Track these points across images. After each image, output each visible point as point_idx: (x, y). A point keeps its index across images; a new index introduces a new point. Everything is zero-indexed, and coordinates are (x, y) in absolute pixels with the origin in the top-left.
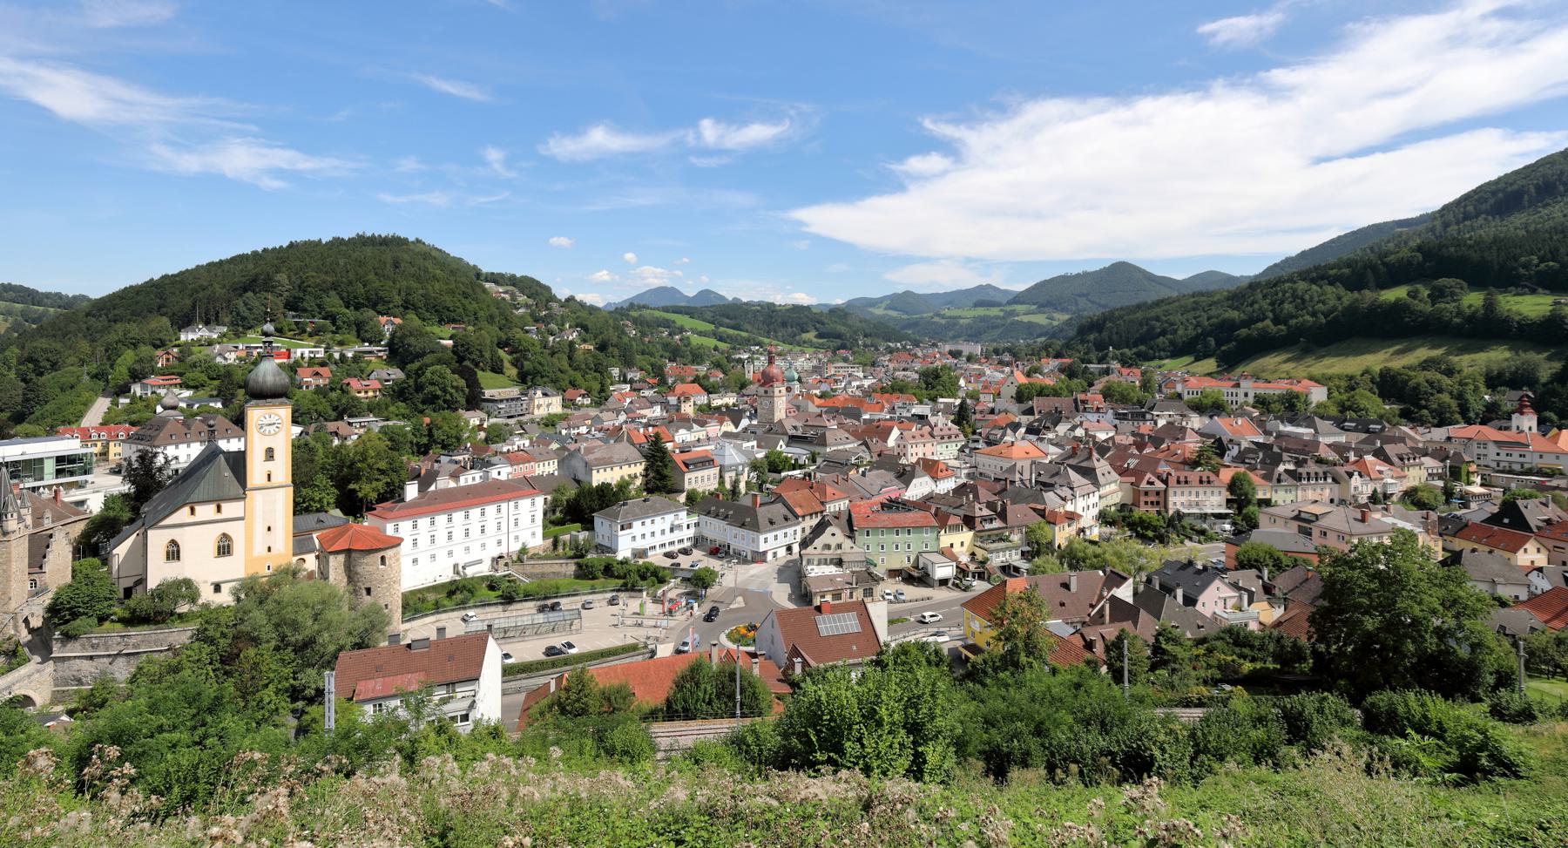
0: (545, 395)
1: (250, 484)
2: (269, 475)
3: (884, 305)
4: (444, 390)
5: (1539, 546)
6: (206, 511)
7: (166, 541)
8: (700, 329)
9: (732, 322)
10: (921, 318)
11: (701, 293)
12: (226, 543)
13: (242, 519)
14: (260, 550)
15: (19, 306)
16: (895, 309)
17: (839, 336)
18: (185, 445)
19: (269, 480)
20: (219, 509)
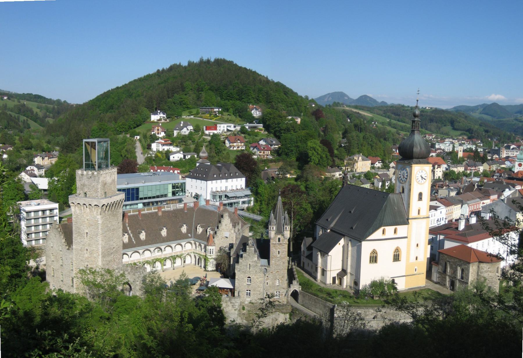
2: (419, 210)
3: (478, 111)
5: (350, 239)
6: (390, 230)
7: (370, 251)
12: (398, 253)
13: (406, 237)
14: (412, 259)
15: (44, 105)
16: (487, 114)
18: (225, 180)
19: (419, 214)
20: (395, 232)
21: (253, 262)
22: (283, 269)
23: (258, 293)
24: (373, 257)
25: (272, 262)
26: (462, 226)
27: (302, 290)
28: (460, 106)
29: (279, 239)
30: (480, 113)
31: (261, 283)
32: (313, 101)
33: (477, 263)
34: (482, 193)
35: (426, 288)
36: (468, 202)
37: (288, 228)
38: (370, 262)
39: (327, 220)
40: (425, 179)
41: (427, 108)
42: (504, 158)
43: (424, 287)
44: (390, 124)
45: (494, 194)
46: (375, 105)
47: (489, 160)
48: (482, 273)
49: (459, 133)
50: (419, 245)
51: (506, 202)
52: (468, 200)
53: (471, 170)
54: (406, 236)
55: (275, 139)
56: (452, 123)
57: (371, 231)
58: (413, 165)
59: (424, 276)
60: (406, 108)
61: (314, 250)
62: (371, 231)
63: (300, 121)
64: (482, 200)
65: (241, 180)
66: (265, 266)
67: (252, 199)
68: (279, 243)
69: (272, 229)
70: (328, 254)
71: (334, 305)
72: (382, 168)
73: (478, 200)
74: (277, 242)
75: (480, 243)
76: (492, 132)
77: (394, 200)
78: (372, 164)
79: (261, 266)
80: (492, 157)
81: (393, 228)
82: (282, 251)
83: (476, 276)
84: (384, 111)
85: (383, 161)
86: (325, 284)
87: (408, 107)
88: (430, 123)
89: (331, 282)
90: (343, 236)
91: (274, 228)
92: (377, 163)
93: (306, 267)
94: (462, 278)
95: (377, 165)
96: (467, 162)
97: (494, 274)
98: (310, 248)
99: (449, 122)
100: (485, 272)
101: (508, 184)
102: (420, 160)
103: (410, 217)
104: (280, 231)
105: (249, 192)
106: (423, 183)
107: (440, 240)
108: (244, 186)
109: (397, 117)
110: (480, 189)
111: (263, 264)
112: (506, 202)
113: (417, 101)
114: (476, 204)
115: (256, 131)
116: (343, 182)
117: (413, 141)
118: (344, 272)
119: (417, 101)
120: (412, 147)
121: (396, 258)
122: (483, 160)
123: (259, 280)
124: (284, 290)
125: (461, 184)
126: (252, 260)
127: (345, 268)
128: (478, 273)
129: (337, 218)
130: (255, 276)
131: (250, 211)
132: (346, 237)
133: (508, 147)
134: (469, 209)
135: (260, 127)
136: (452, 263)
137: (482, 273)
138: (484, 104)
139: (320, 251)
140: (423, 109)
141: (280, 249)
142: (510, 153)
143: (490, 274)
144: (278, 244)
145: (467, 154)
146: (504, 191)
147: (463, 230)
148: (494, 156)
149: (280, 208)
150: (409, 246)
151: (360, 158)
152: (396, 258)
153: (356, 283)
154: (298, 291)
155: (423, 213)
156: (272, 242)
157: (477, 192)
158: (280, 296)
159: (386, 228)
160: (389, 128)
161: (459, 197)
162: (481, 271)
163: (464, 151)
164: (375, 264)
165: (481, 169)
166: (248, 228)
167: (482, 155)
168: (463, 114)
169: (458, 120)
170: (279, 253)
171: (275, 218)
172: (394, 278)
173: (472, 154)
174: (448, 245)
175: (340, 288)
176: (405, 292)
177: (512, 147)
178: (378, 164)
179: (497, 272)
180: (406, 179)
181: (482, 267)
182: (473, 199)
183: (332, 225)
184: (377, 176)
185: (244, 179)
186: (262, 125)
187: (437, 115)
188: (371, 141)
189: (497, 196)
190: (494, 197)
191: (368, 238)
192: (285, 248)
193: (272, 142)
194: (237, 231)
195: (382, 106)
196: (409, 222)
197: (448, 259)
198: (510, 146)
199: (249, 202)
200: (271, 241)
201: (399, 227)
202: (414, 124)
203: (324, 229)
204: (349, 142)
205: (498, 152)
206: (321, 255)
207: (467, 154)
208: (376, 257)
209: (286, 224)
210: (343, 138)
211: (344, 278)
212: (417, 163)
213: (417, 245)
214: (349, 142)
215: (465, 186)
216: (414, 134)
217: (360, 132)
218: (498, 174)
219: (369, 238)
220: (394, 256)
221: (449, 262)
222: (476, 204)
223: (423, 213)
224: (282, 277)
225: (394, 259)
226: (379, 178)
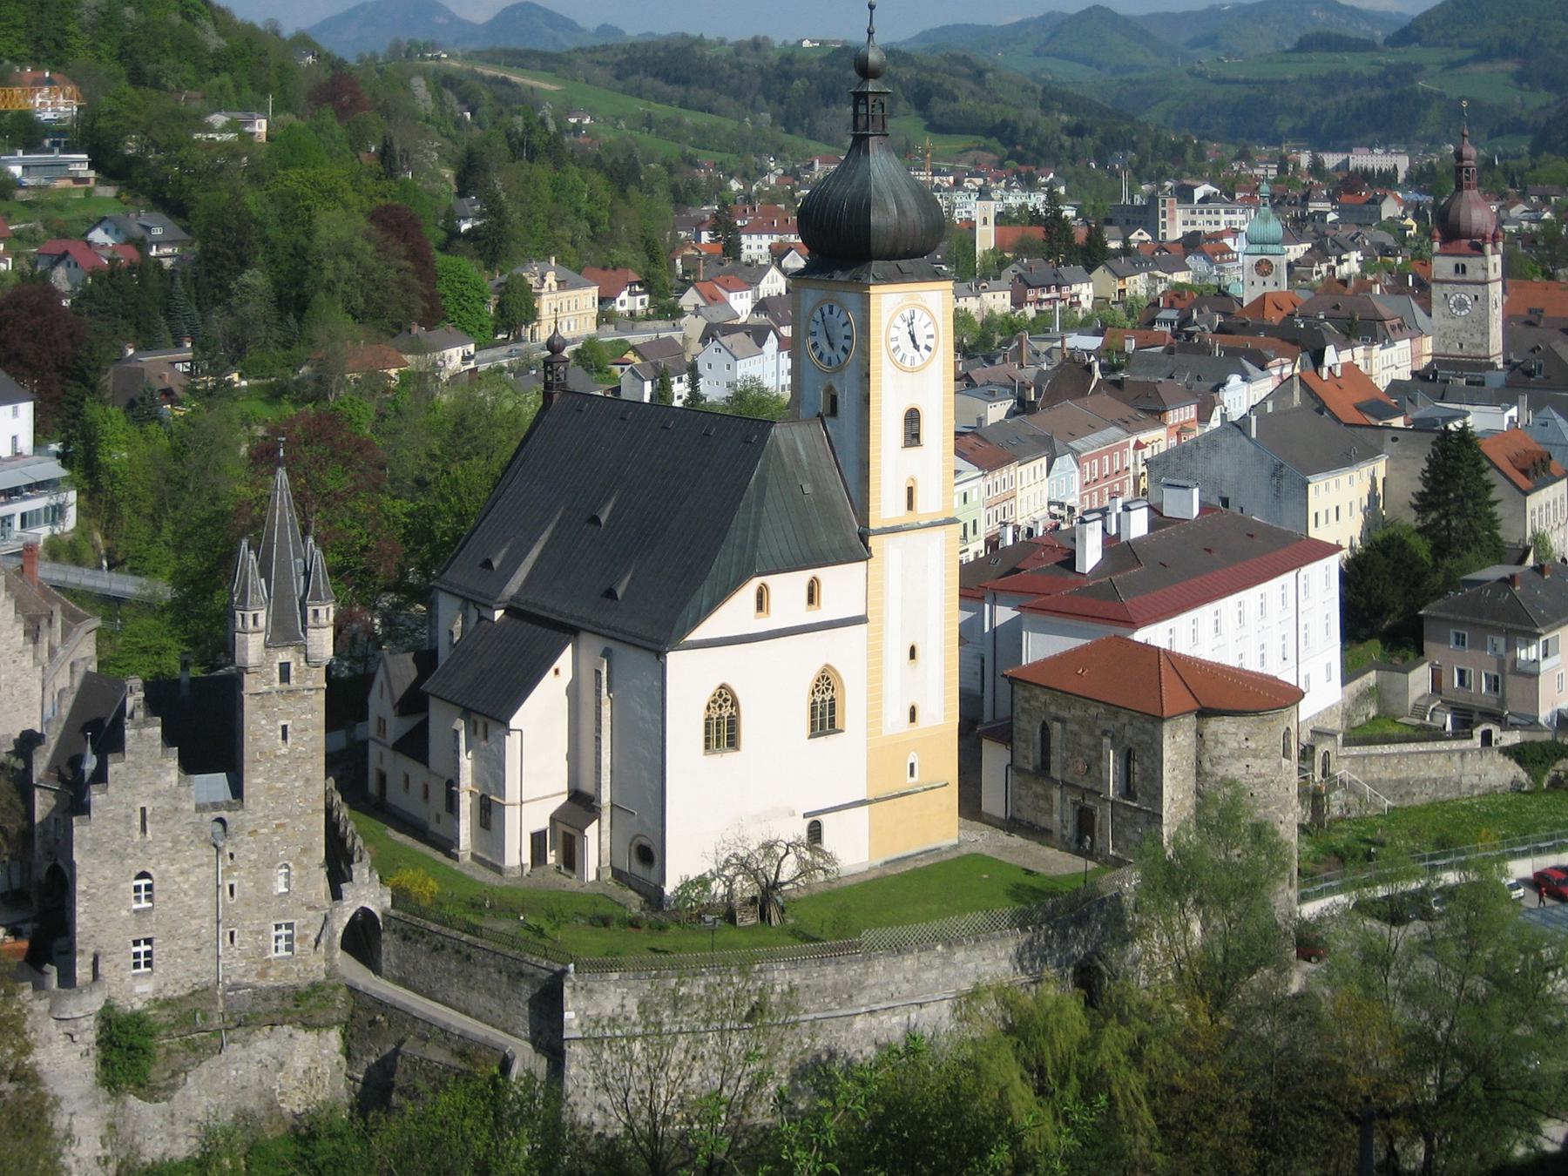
2: (910, 490)
6: (787, 588)
12: (827, 697)
19: (910, 506)
20: (812, 597)
21: (156, 795)
22: (303, 813)
23: (191, 944)
24: (718, 724)
25: (254, 780)
26: (1091, 555)
27: (393, 906)
28: (944, 30)
29: (285, 670)
30: (1037, 53)
31: (199, 894)
32: (303, 41)
33: (1193, 718)
34: (1126, 402)
35: (965, 850)
36: (1075, 444)
37: (327, 612)
38: (707, 747)
39: (488, 564)
40: (928, 348)
41: (806, 44)
42: (1177, 241)
43: (956, 847)
45: (1180, 403)
47: (1116, 254)
48: (1215, 762)
49: (959, 142)
50: (918, 653)
51: (1254, 435)
52: (1073, 436)
53: (1040, 301)
54: (860, 612)
55: (160, 216)
56: (921, 98)
57: (703, 595)
58: (873, 290)
59: (951, 796)
61: (436, 711)
62: (705, 603)
63: (264, 129)
64: (1130, 433)
65: (15, 414)
66: (215, 806)
67: (72, 496)
68: (285, 686)
69: (250, 622)
70: (505, 723)
71: (558, 967)
72: (648, 318)
73: (1114, 431)
74: (277, 684)
75: (1182, 622)
76: (1099, 131)
77: (795, 450)
78: (601, 301)
79: (200, 808)
80: (1126, 241)
81: (802, 578)
82: (300, 726)
83: (1192, 780)
84: (618, 65)
85: (648, 285)
86: (498, 870)
87: (722, 42)
88: (823, 110)
89: (527, 859)
90: (568, 631)
91: (262, 621)
92: (624, 295)
93: (395, 795)
94: (1128, 791)
95: (622, 303)
96: (1020, 270)
97: (1274, 764)
98: (413, 702)
99: (908, 99)
100: (1232, 756)
101: (1232, 353)
102: (904, 264)
103: (873, 525)
104: (286, 631)
105: (54, 470)
106: (923, 367)
107: (994, 631)
108: (26, 443)
109: (679, 91)
110: (1118, 384)
111: (205, 799)
112: (1254, 435)
113: (871, 7)
114: (1110, 452)
115: (60, 184)
116: (548, 386)
117: (866, 183)
118: (581, 803)
120: (862, 208)
121: (824, 720)
122: (1091, 256)
123: (193, 879)
124: (311, 913)
125: (1021, 366)
126: (151, 789)
127: (587, 786)
128: (1199, 762)
129: (535, 553)
130: (172, 862)
131: (63, 557)
132: (586, 640)
133: (1184, 195)
134: (1083, 473)
135: (77, 167)
136: (1075, 727)
137: (1215, 762)
138: (1049, 16)
139: (467, 713)
141: (288, 715)
142: (1200, 219)
143: (1257, 766)
144: (279, 692)
145: (1014, 233)
146: (1223, 385)
148: (1133, 236)
149: (282, 527)
150: (875, 654)
151: (551, 278)
152: (824, 720)
153: (649, 854)
154: (379, 915)
155: (930, 504)
156: (250, 684)
157: (1105, 398)
158: (297, 946)
159: (772, 581)
160: (647, 140)
161: (1033, 423)
162: (1216, 753)
163: (1002, 219)
164: (730, 757)
165: (1085, 293)
166: (93, 635)
167: (1080, 234)
168: (965, 61)
169: (947, 86)
170: (285, 737)
171: (265, 571)
172: (821, 818)
173: (1038, 233)
174: (1038, 647)
175: (572, 883)
176: (870, 877)
177: (1199, 193)
178: (629, 302)
179: (1286, 753)
180: (845, 350)
181: (1215, 734)
182: (1093, 428)
183: (513, 587)
184: (630, 356)
185: (26, 409)
186: (85, 156)
188: (591, 197)
189: (1193, 408)
190: (1183, 414)
191: (695, 636)
192: (312, 711)
193: (148, 229)
194: (44, 654)
195: (605, 48)
196: (868, 549)
197: (1053, 709)
198: (1191, 189)
199: (57, 512)
200: (248, 680)
201: (830, 576)
202: (862, 110)
203: (476, 602)
204: (494, 210)
205: (1147, 216)
206: (472, 732)
207: (1014, 233)
208: (733, 724)
209: (317, 597)
210: (462, 194)
211: (588, 831)
212: (888, 279)
213: (912, 653)
214: (494, 210)
215: (1041, 373)
216: (867, 152)
217: (531, 160)
218: (1172, 314)
219: (697, 635)
220: (813, 709)
221: (1063, 721)
222: (1110, 452)
223: (930, 504)
224: (304, 851)
225: (813, 723)
226: (638, 361)
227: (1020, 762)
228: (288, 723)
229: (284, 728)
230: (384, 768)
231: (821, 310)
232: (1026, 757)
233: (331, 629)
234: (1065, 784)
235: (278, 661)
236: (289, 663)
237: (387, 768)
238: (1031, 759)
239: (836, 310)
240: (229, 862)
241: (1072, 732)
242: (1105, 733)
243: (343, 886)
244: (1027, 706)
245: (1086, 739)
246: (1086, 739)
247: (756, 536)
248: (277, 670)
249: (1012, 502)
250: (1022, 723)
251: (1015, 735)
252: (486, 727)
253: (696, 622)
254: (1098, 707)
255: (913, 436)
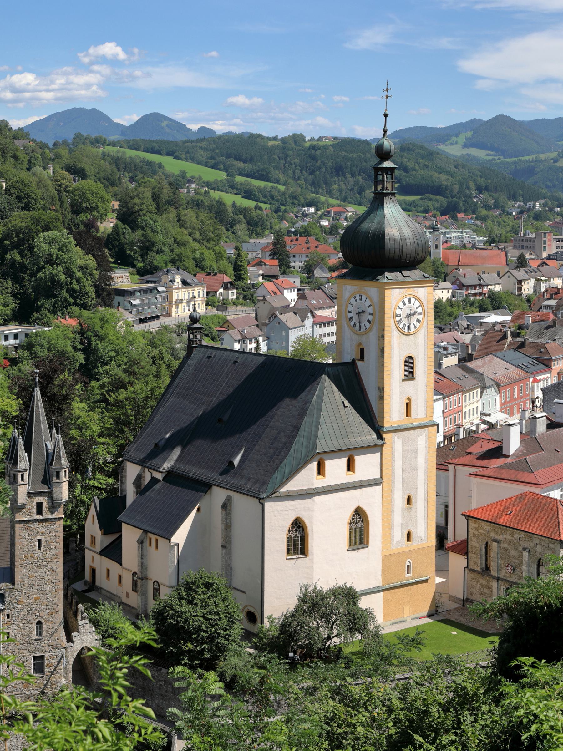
0: (185, 283)
1: (387, 425)
3: (461, 139)
4: (69, 273)
8: (206, 178)
9: (249, 167)
10: (537, 161)
11: (145, 119)
14: (399, 535)
17: (438, 190)
19: (408, 414)
20: (350, 467)
44: (232, 187)
46: (180, 138)
50: (413, 500)
60: (270, 144)
87: (275, 138)
109: (249, 167)
113: (386, 116)
117: (382, 223)
119: (386, 116)
136: (506, 546)
140: (314, 143)
147: (518, 453)
170: (39, 547)
187: (355, 155)
197: (492, 535)
225: (350, 541)
227: (472, 566)
228: (42, 538)
229: (39, 541)
230: (94, 565)
231: (355, 298)
232: (476, 563)
233: (67, 483)
234: (498, 579)
235: (36, 502)
236: (42, 503)
237: (96, 565)
238: (478, 563)
239: (364, 298)
240: (7, 620)
241: (504, 548)
242: (524, 549)
243: (74, 634)
244: (476, 532)
245: (513, 553)
246: (513, 553)
247: (317, 432)
248: (35, 507)
249: (460, 413)
250: (473, 543)
251: (470, 550)
252: (157, 540)
253: (283, 483)
254: (520, 534)
255: (410, 374)
